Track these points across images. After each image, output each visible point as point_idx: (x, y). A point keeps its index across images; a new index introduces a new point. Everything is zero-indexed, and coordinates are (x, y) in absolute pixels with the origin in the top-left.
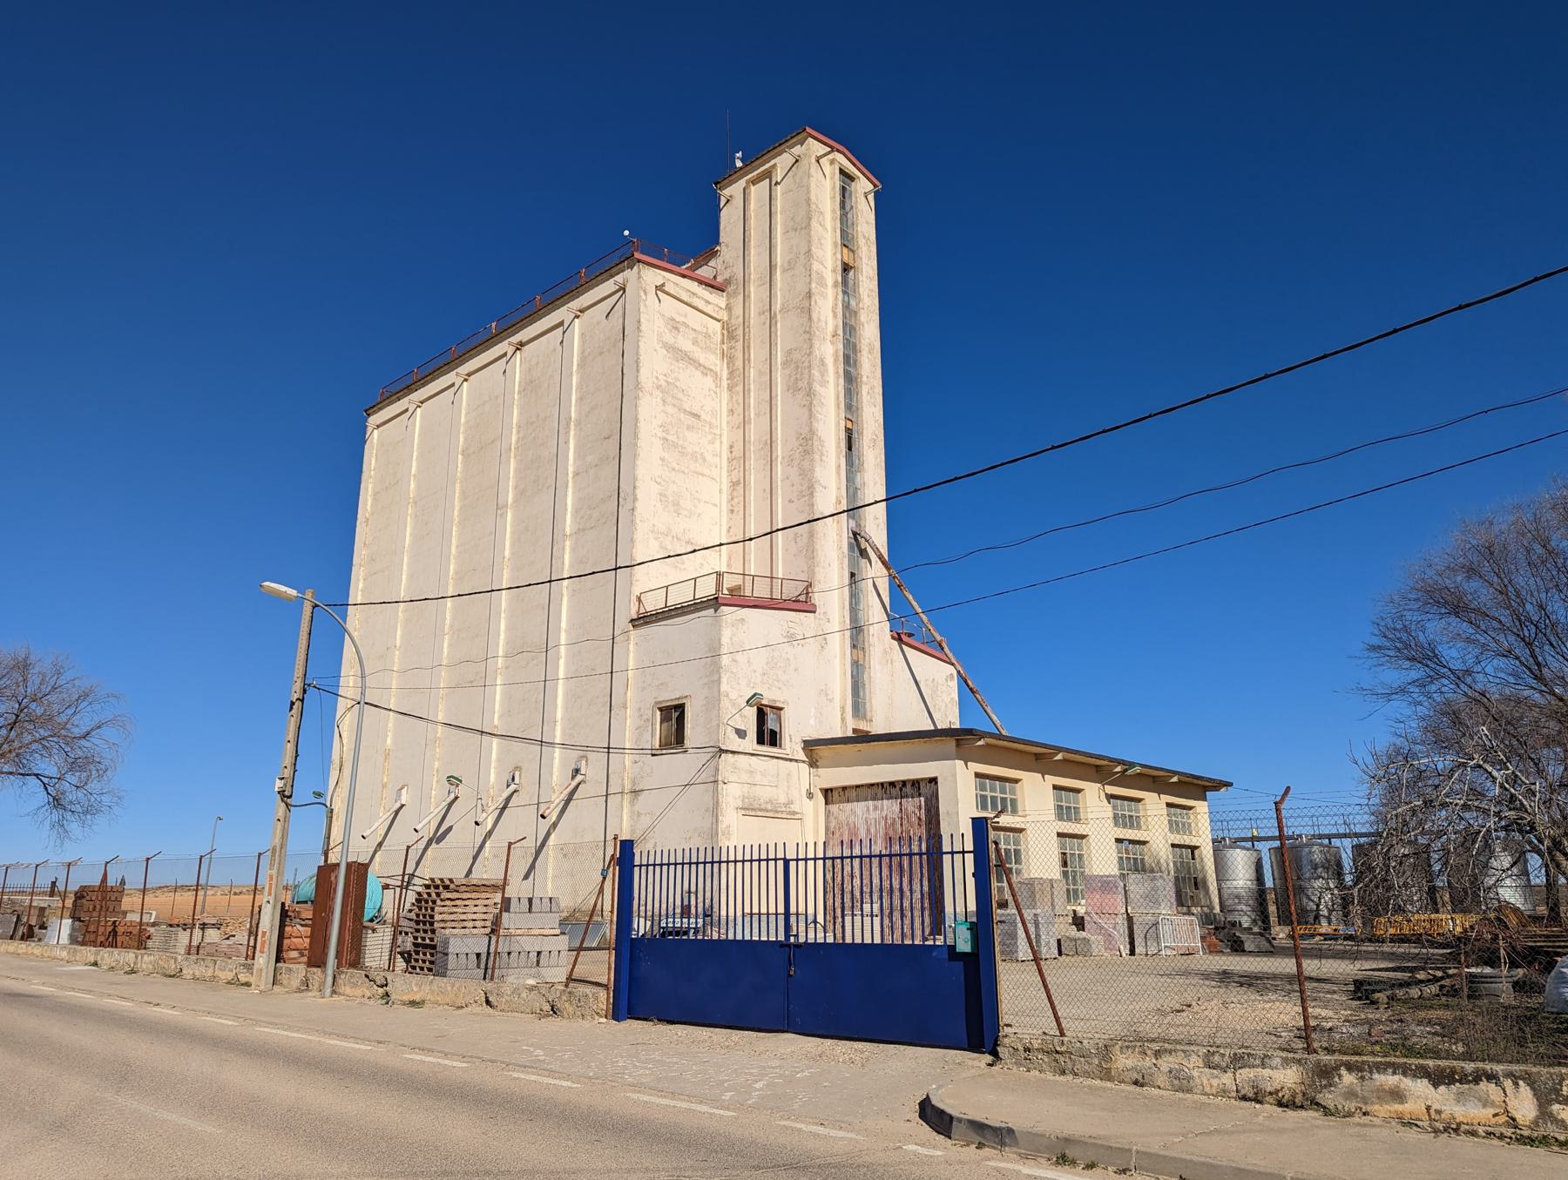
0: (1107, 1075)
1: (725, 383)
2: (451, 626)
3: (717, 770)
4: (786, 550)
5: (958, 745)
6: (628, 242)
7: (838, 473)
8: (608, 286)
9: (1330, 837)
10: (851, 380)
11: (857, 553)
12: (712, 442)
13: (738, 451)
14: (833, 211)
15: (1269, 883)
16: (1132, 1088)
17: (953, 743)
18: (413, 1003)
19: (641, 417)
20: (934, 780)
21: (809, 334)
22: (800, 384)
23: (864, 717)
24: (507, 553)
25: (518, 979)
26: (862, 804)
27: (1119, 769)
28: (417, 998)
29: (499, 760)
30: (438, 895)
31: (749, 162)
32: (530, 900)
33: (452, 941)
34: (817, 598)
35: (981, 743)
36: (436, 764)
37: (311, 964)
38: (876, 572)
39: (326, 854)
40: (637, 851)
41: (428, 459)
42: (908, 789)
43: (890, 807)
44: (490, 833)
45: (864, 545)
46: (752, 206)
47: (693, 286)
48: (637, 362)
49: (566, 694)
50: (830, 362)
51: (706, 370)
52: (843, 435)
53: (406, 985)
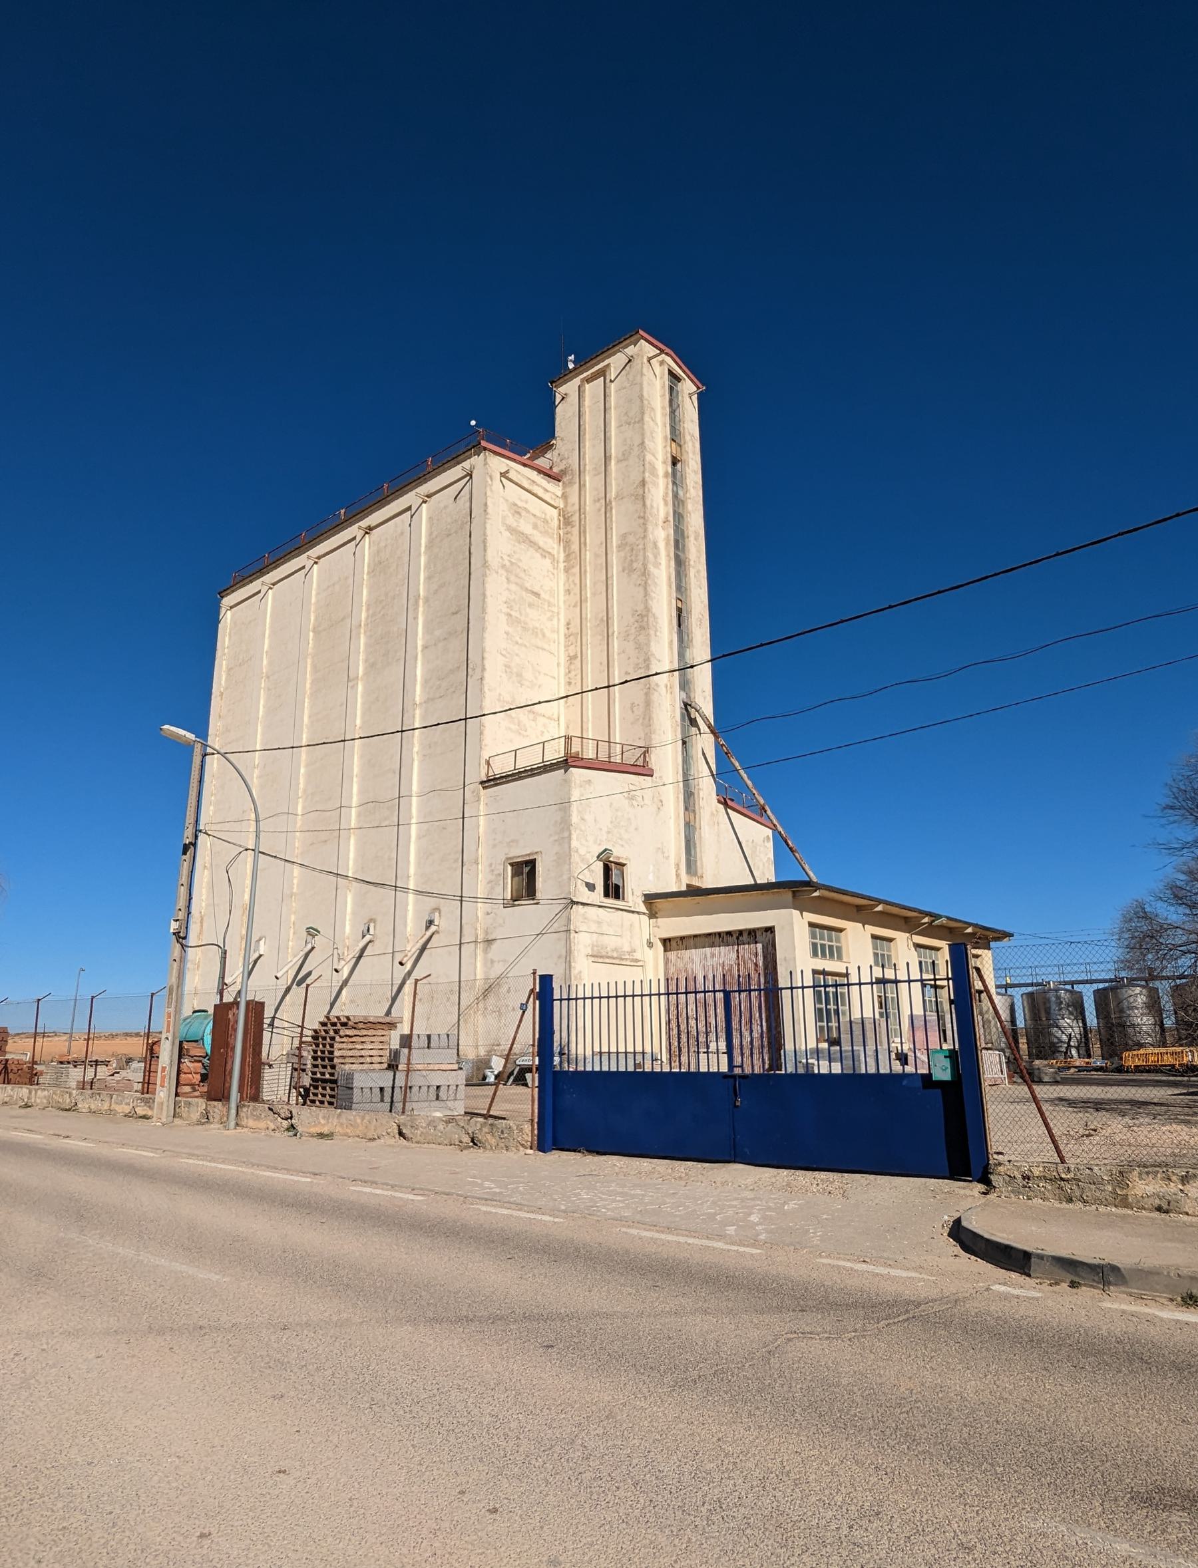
0: (1124, 1203)
1: (562, 565)
2: (305, 791)
3: (569, 920)
4: (623, 719)
5: (794, 896)
6: (473, 431)
7: (671, 648)
8: (456, 472)
9: (1072, 983)
10: (680, 563)
11: (687, 722)
12: (550, 619)
13: (575, 628)
14: (663, 408)
15: (1021, 1023)
16: (1156, 1215)
17: (790, 895)
18: (321, 1135)
19: (488, 593)
20: (771, 930)
21: (643, 520)
22: (635, 565)
23: (695, 874)
24: (358, 722)
25: (427, 1112)
26: (700, 951)
27: (926, 920)
28: (326, 1130)
29: (354, 913)
30: (336, 1032)
31: (582, 363)
32: (429, 1037)
33: (356, 1076)
34: (654, 760)
35: (816, 894)
36: (293, 918)
37: (211, 1097)
38: (705, 742)
39: (221, 993)
40: (556, 986)
41: (283, 638)
42: (745, 937)
43: (727, 954)
44: (345, 982)
45: (694, 714)
46: (587, 402)
47: (534, 475)
48: (485, 542)
49: (418, 853)
50: (662, 545)
51: (545, 553)
52: (675, 613)
53: (313, 1118)
